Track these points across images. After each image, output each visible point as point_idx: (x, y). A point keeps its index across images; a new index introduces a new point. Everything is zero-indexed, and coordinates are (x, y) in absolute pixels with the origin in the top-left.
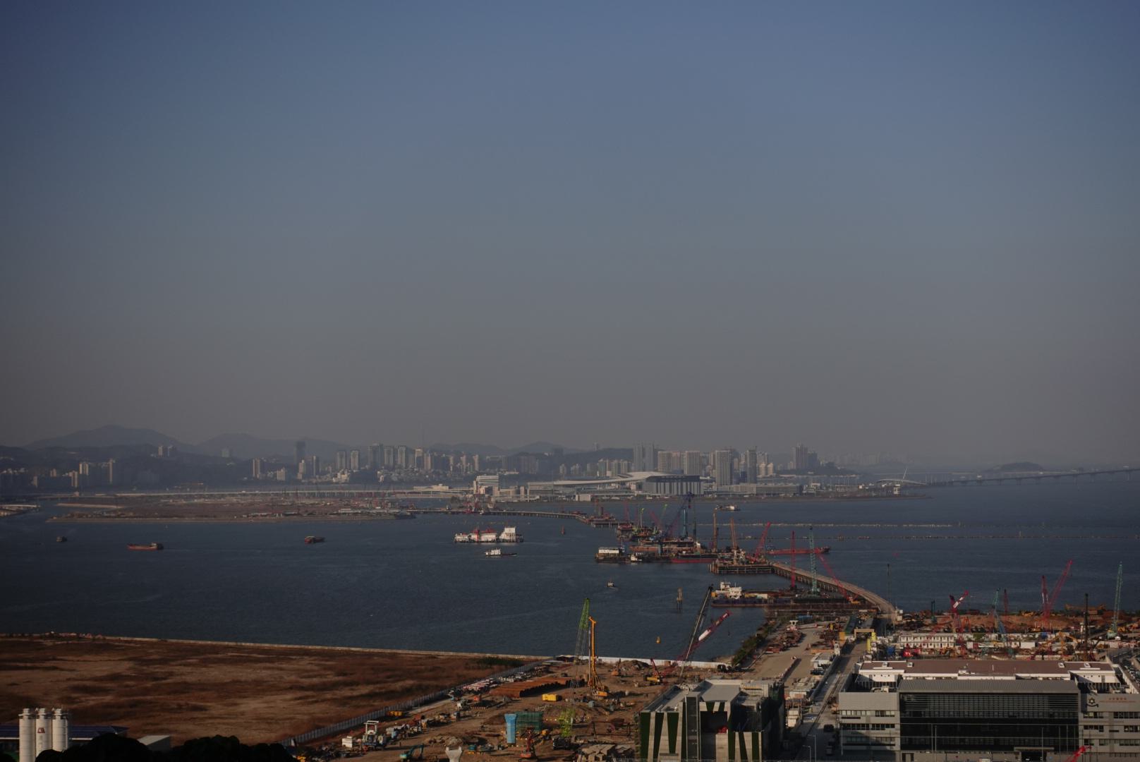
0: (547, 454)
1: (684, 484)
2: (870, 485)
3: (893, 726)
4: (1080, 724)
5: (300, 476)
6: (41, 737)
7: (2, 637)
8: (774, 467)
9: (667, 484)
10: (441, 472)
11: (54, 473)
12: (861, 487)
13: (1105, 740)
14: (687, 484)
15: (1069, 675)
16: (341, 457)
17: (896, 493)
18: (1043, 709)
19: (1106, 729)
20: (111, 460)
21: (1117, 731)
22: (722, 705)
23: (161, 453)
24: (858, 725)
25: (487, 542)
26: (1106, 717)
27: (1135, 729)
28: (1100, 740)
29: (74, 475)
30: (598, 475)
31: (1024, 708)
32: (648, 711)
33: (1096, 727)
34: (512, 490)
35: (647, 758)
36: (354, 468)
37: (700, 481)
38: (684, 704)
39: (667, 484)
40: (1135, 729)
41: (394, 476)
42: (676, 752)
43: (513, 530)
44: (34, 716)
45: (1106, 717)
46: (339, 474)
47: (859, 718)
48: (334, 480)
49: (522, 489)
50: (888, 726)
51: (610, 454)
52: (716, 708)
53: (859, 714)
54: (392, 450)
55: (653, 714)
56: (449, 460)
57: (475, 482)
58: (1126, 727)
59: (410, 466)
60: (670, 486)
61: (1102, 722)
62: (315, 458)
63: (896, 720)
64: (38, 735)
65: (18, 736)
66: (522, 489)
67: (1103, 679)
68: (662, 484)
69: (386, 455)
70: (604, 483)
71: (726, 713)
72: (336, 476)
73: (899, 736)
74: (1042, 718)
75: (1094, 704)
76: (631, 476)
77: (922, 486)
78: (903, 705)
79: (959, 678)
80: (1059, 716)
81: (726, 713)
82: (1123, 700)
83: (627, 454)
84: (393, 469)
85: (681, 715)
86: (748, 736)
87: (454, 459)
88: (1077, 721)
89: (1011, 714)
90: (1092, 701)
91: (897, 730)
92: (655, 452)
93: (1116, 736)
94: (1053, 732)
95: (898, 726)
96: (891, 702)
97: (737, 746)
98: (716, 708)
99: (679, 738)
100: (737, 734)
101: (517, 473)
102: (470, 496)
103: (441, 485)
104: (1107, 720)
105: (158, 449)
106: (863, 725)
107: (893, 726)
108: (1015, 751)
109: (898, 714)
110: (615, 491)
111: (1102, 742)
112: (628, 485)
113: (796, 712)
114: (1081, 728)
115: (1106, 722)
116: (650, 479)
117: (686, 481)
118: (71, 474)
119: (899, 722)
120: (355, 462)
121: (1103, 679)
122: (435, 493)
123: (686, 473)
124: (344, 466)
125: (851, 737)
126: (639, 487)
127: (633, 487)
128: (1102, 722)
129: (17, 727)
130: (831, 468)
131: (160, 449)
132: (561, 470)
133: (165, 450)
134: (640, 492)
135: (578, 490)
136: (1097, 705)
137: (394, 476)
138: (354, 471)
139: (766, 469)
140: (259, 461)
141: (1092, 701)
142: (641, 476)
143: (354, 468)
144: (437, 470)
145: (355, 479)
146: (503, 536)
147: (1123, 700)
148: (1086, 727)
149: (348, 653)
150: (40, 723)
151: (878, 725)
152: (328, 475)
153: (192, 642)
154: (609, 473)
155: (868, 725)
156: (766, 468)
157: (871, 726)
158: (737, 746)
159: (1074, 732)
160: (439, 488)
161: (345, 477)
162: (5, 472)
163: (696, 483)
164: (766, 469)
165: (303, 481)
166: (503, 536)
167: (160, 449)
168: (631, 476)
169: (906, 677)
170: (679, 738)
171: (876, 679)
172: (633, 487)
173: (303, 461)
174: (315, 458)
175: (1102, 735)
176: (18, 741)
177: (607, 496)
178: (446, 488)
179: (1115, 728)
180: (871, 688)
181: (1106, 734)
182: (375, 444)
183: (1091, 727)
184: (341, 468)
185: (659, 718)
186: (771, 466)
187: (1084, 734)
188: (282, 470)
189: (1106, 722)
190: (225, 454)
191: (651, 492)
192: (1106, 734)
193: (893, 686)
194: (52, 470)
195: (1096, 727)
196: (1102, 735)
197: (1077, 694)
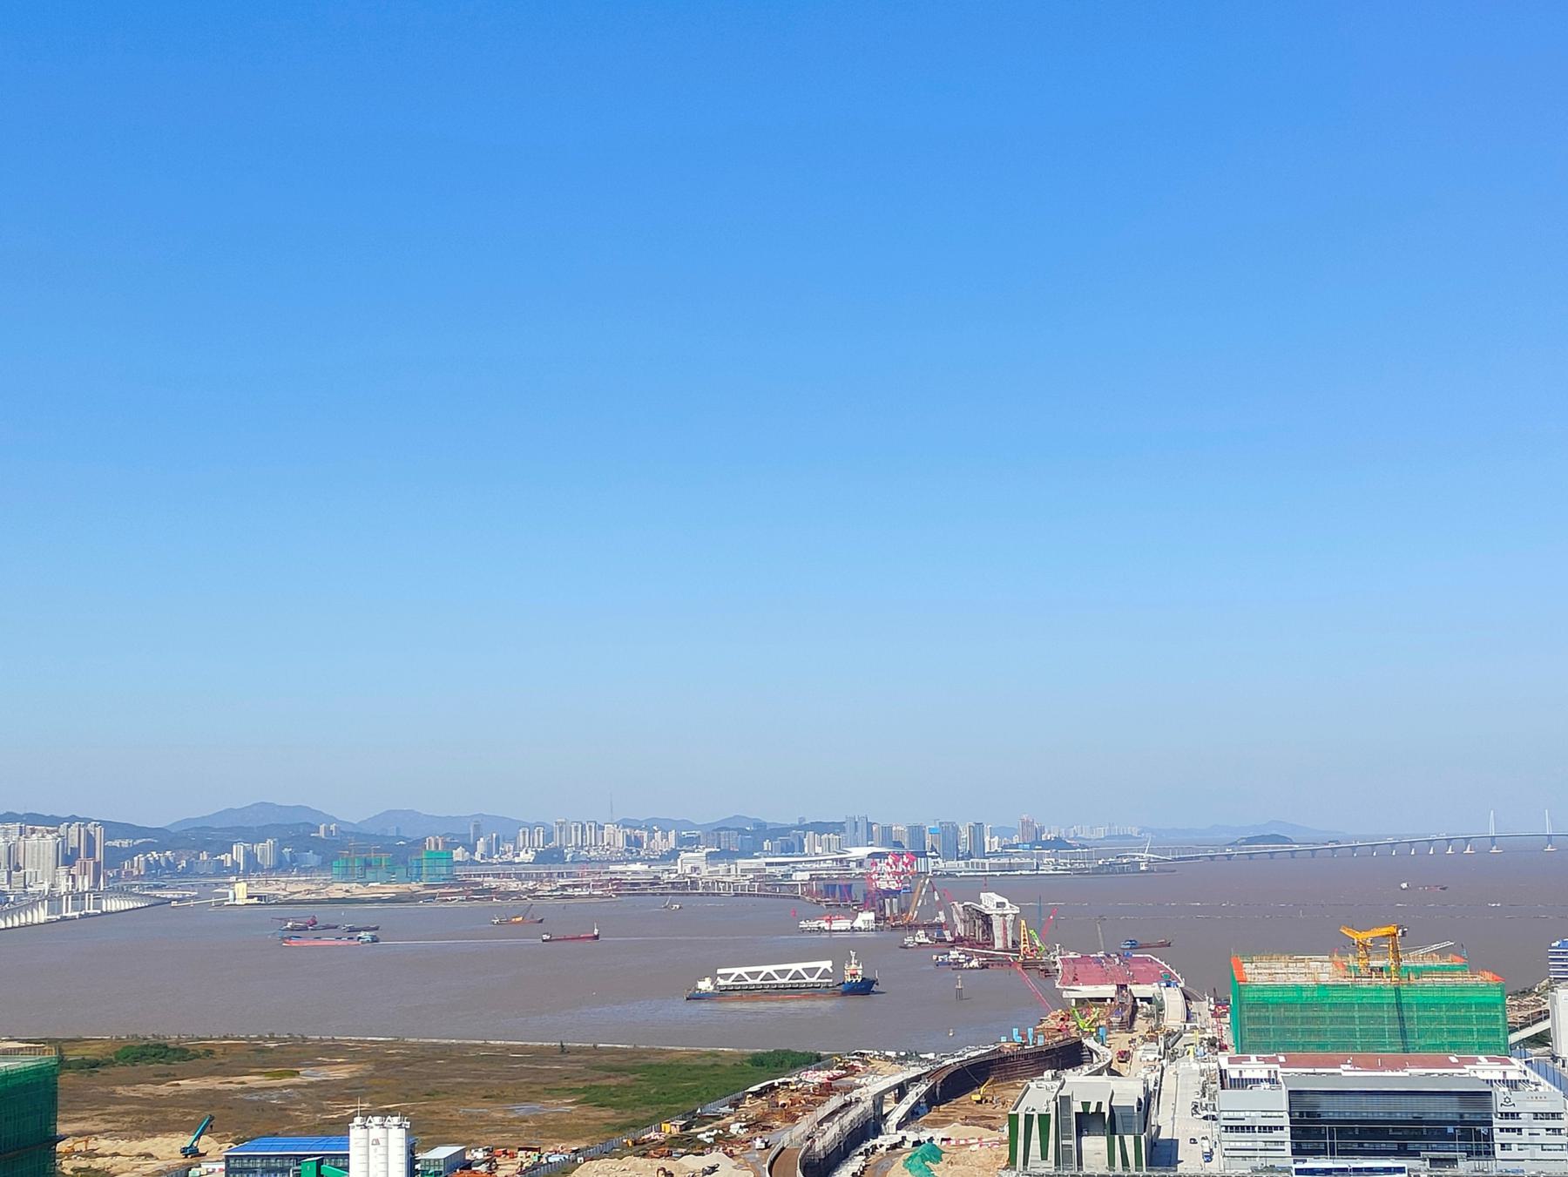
0: (748, 829)
1: (109, 909)
4: (1494, 1126)
7: (6, 1053)
12: (1100, 862)
17: (1143, 868)
20: (269, 840)
21: (1538, 1134)
22: (1099, 1104)
24: (1243, 1127)
27: (1557, 1131)
34: (722, 867)
36: (539, 847)
37: (926, 856)
38: (1057, 1103)
40: (1557, 1131)
46: (521, 853)
49: (733, 867)
50: (1276, 1128)
51: (820, 828)
52: (1092, 1109)
54: (580, 826)
62: (494, 835)
63: (1286, 1121)
66: (733, 867)
69: (573, 832)
70: (820, 860)
73: (1289, 1140)
76: (850, 852)
79: (1344, 1074)
81: (1104, 1113)
82: (1543, 1099)
83: (837, 828)
85: (1053, 1117)
86: (1129, 1140)
91: (1287, 1132)
92: (870, 825)
93: (1537, 1140)
94: (1466, 1136)
95: (1288, 1129)
98: (1092, 1109)
99: (1052, 1143)
106: (1248, 1127)
111: (1521, 1147)
118: (223, 857)
120: (539, 840)
126: (860, 863)
133: (327, 830)
134: (862, 871)
136: (1514, 1105)
141: (1507, 1100)
142: (861, 852)
143: (539, 847)
145: (540, 858)
147: (1543, 1099)
152: (510, 854)
153: (435, 1041)
155: (1253, 1127)
156: (992, 843)
157: (1256, 1129)
159: (1489, 1137)
163: (923, 859)
168: (850, 852)
170: (1052, 1143)
172: (853, 865)
174: (494, 835)
175: (1521, 1139)
177: (826, 874)
178: (645, 867)
179: (1535, 1131)
180: (1247, 1085)
184: (524, 846)
187: (1499, 1138)
195: (1513, 1130)
196: (1521, 1139)
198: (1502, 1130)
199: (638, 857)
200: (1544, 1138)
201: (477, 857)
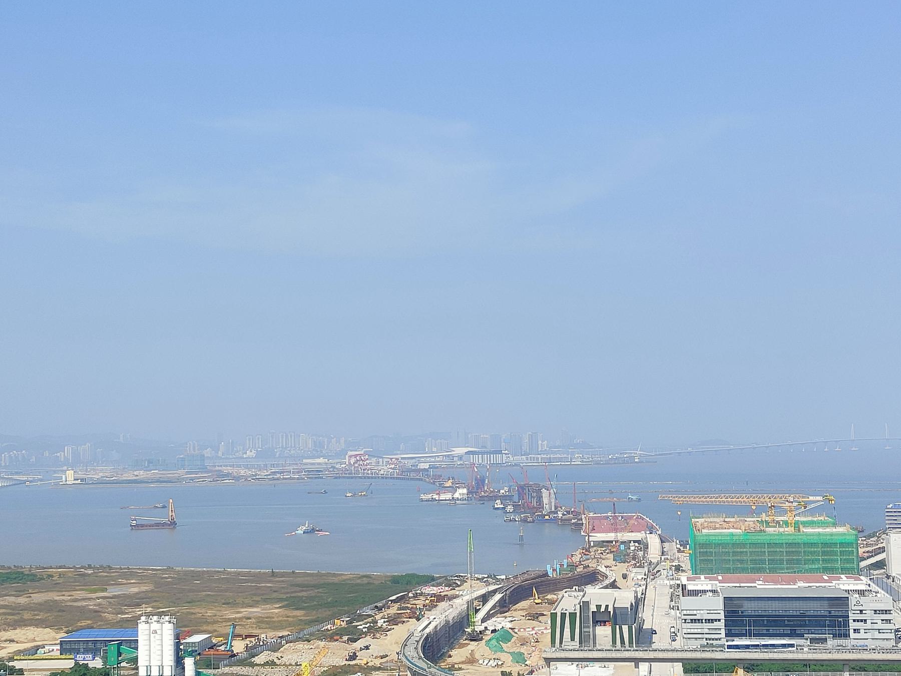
1: (492, 455)
2: (616, 455)
3: (719, 620)
4: (850, 618)
9: (480, 456)
14: (493, 456)
16: (249, 439)
18: (821, 609)
19: (869, 622)
22: (607, 606)
24: (695, 620)
25: (446, 500)
28: (865, 629)
30: (427, 450)
33: (862, 621)
37: (502, 453)
38: (580, 606)
43: (465, 491)
50: (716, 620)
56: (324, 442)
58: (882, 620)
60: (482, 457)
61: (866, 617)
63: (722, 616)
68: (477, 456)
75: (859, 604)
76: (454, 451)
79: (758, 587)
81: (610, 612)
82: (880, 601)
86: (625, 628)
93: (876, 627)
94: (832, 625)
98: (603, 609)
100: (618, 626)
102: (344, 466)
106: (699, 620)
107: (719, 620)
114: (851, 621)
115: (868, 617)
116: (468, 453)
117: (493, 454)
118: (58, 454)
122: (319, 464)
124: (251, 447)
126: (460, 458)
128: (866, 617)
132: (401, 447)
136: (862, 605)
141: (858, 602)
146: (457, 495)
147: (880, 601)
148: (854, 621)
149: (53, 571)
151: (709, 620)
152: (240, 452)
155: (702, 620)
159: (846, 624)
160: (321, 460)
166: (457, 495)
168: (454, 451)
175: (866, 626)
179: (875, 621)
181: (869, 625)
183: (858, 621)
187: (853, 625)
189: (868, 617)
192: (869, 625)
194: (45, 451)
195: (862, 621)
196: (866, 626)
198: (854, 621)
199: (245, 456)
200: (880, 625)
201: (220, 454)
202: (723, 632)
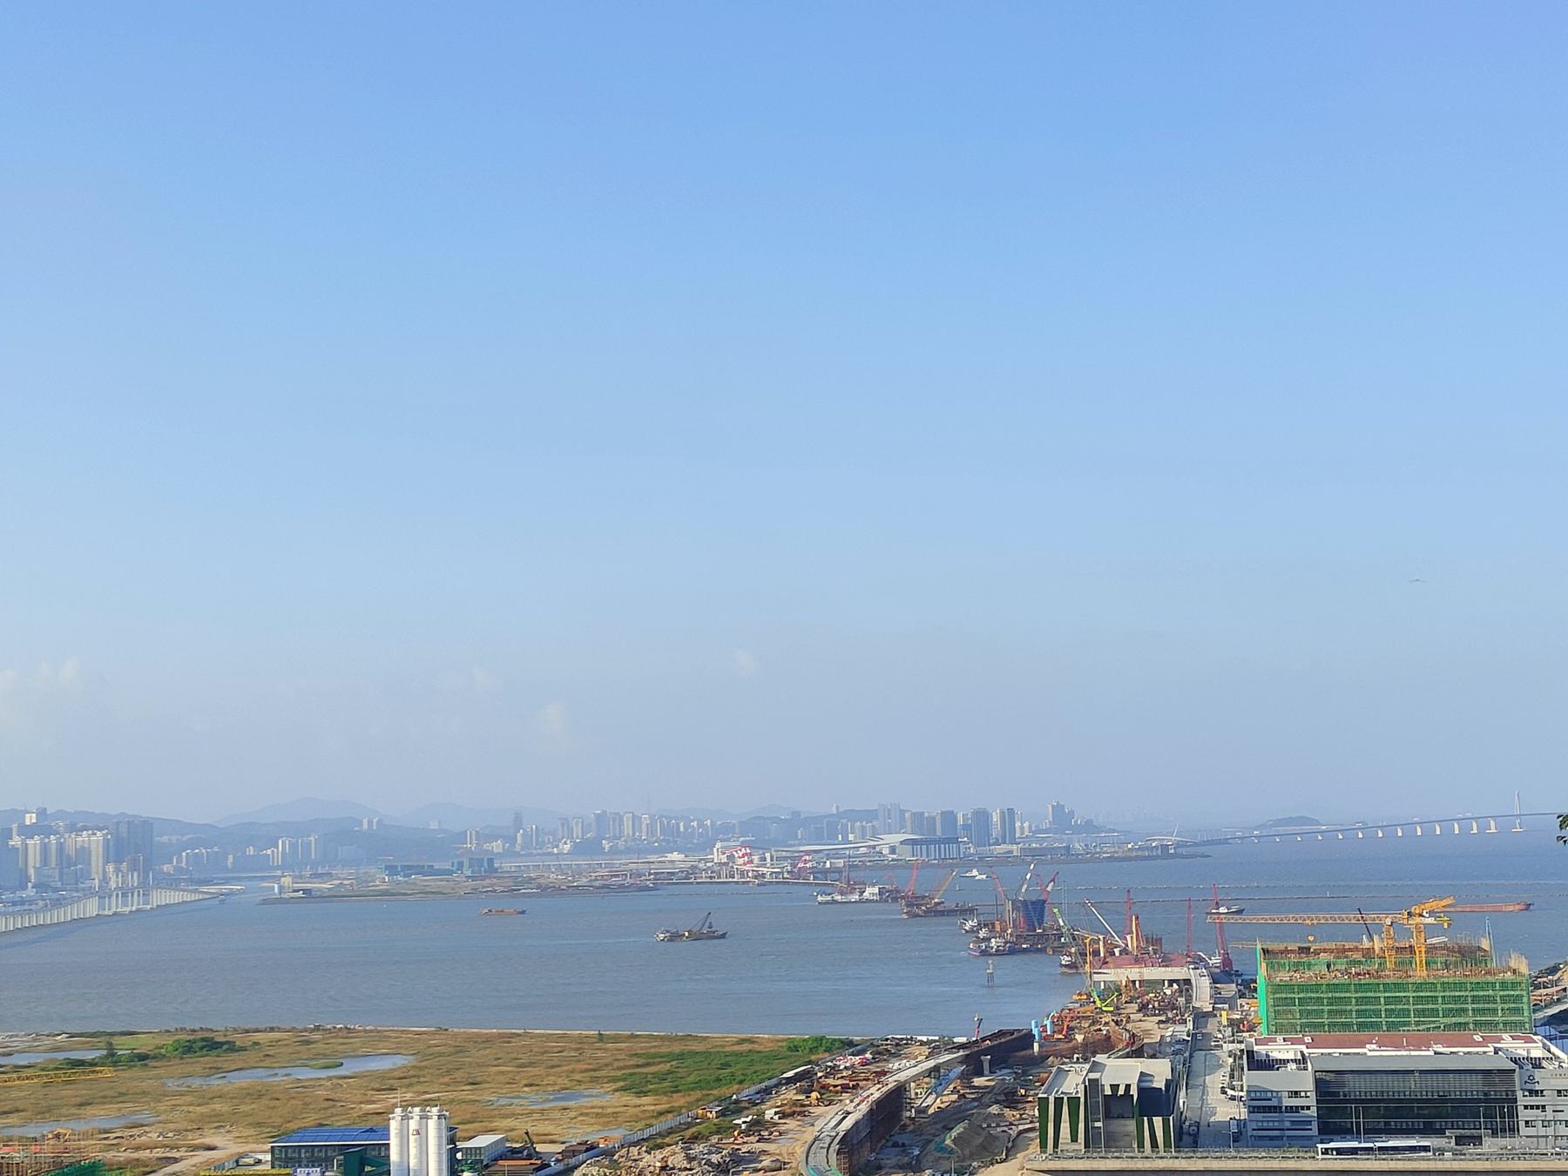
4: (1519, 1103)
5: (518, 848)
6: (416, 1139)
8: (1030, 827)
9: (924, 847)
10: (671, 839)
11: (251, 851)
13: (1549, 1121)
15: (1492, 1049)
18: (1475, 1086)
21: (1563, 1111)
22: (1128, 1087)
23: (365, 826)
26: (1548, 1096)
29: (273, 851)
31: (1421, 1087)
32: (1045, 1096)
35: (1046, 1148)
36: (577, 838)
39: (924, 847)
41: (621, 844)
42: (1079, 1141)
44: (406, 1118)
45: (1548, 1096)
47: (1271, 1100)
48: (555, 850)
51: (852, 815)
52: (1121, 1092)
53: (1269, 1095)
54: (617, 817)
55: (1051, 1100)
57: (715, 850)
59: (637, 834)
62: (534, 827)
64: (412, 1138)
65: (389, 1140)
67: (1528, 1052)
71: (1133, 1095)
72: (557, 846)
74: (1409, 1097)
77: (1196, 844)
78: (1319, 1084)
79: (1369, 1054)
80: (1472, 1095)
81: (1133, 1095)
84: (619, 838)
85: (1082, 1100)
86: (1158, 1121)
87: (684, 826)
88: (1515, 1101)
89: (1441, 1094)
90: (1531, 1078)
96: (1307, 1083)
97: (1147, 1134)
98: (1121, 1092)
99: (1081, 1126)
101: (753, 839)
103: (675, 853)
104: (1550, 1098)
105: (362, 821)
106: (1275, 1107)
108: (1447, 1134)
109: (1313, 1095)
110: (864, 855)
112: (878, 849)
113: (1119, 1093)
114: (1521, 1108)
118: (269, 852)
119: (1315, 1104)
120: (577, 831)
121: (1528, 1052)
123: (939, 833)
124: (566, 835)
125: (1262, 1121)
126: (893, 850)
127: (886, 851)
129: (387, 1129)
130: (1089, 827)
131: (365, 821)
133: (370, 822)
135: (828, 855)
137: (621, 844)
138: (578, 841)
139: (1022, 828)
140: (474, 832)
142: (895, 839)
144: (667, 838)
145: (578, 850)
150: (413, 1125)
154: (851, 837)
156: (1022, 827)
158: (1147, 1134)
159: (1513, 1113)
160: (675, 856)
161: (567, 847)
162: (197, 851)
164: (1022, 828)
165: (522, 853)
167: (365, 821)
169: (1310, 1054)
170: (1081, 1126)
171: (1276, 1055)
172: (886, 851)
173: (521, 831)
174: (534, 827)
176: (389, 1144)
180: (1274, 1066)
182: (599, 812)
185: (1058, 1101)
186: (1026, 825)
187: (1524, 1115)
188: (499, 842)
190: (434, 825)
191: (906, 854)
193: (1302, 1061)
195: (1538, 1107)
197: (1515, 1070)
202: (1315, 1126)
